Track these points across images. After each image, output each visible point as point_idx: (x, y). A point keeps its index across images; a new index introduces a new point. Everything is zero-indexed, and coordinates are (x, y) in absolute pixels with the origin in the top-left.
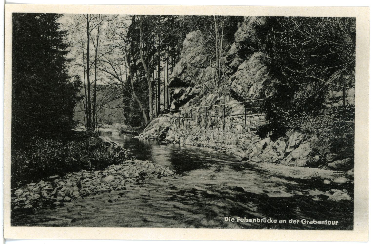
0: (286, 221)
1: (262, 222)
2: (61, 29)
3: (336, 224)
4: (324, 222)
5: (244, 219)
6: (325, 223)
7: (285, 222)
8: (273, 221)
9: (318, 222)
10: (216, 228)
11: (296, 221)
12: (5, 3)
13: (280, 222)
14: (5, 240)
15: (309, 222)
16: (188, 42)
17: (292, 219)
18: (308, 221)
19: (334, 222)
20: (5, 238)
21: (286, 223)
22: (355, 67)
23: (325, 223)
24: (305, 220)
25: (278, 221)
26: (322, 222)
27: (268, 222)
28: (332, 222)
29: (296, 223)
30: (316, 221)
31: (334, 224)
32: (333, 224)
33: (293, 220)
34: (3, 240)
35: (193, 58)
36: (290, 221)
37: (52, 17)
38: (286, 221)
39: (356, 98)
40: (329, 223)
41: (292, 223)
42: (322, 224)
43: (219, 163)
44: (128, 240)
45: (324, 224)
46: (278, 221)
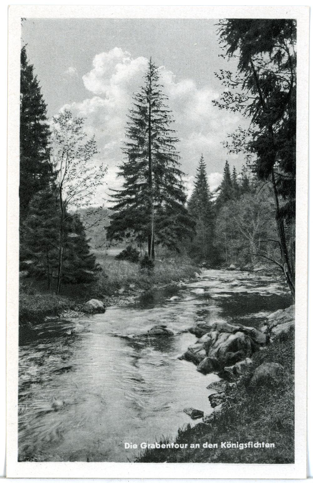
0: (216, 445)
2: (110, 220)
3: (186, 447)
5: (236, 444)
6: (262, 445)
7: (272, 445)
8: (226, 445)
11: (165, 446)
13: (191, 447)
14: (308, 477)
15: (150, 447)
16: (257, 63)
17: (207, 443)
19: (183, 445)
20: (305, 477)
21: (199, 447)
23: (262, 445)
25: (189, 446)
27: (255, 447)
28: (181, 445)
34: (309, 480)
35: (97, 224)
36: (204, 445)
38: (216, 445)
39: (300, 69)
40: (177, 446)
42: (233, 447)
43: (199, 350)
45: (235, 447)
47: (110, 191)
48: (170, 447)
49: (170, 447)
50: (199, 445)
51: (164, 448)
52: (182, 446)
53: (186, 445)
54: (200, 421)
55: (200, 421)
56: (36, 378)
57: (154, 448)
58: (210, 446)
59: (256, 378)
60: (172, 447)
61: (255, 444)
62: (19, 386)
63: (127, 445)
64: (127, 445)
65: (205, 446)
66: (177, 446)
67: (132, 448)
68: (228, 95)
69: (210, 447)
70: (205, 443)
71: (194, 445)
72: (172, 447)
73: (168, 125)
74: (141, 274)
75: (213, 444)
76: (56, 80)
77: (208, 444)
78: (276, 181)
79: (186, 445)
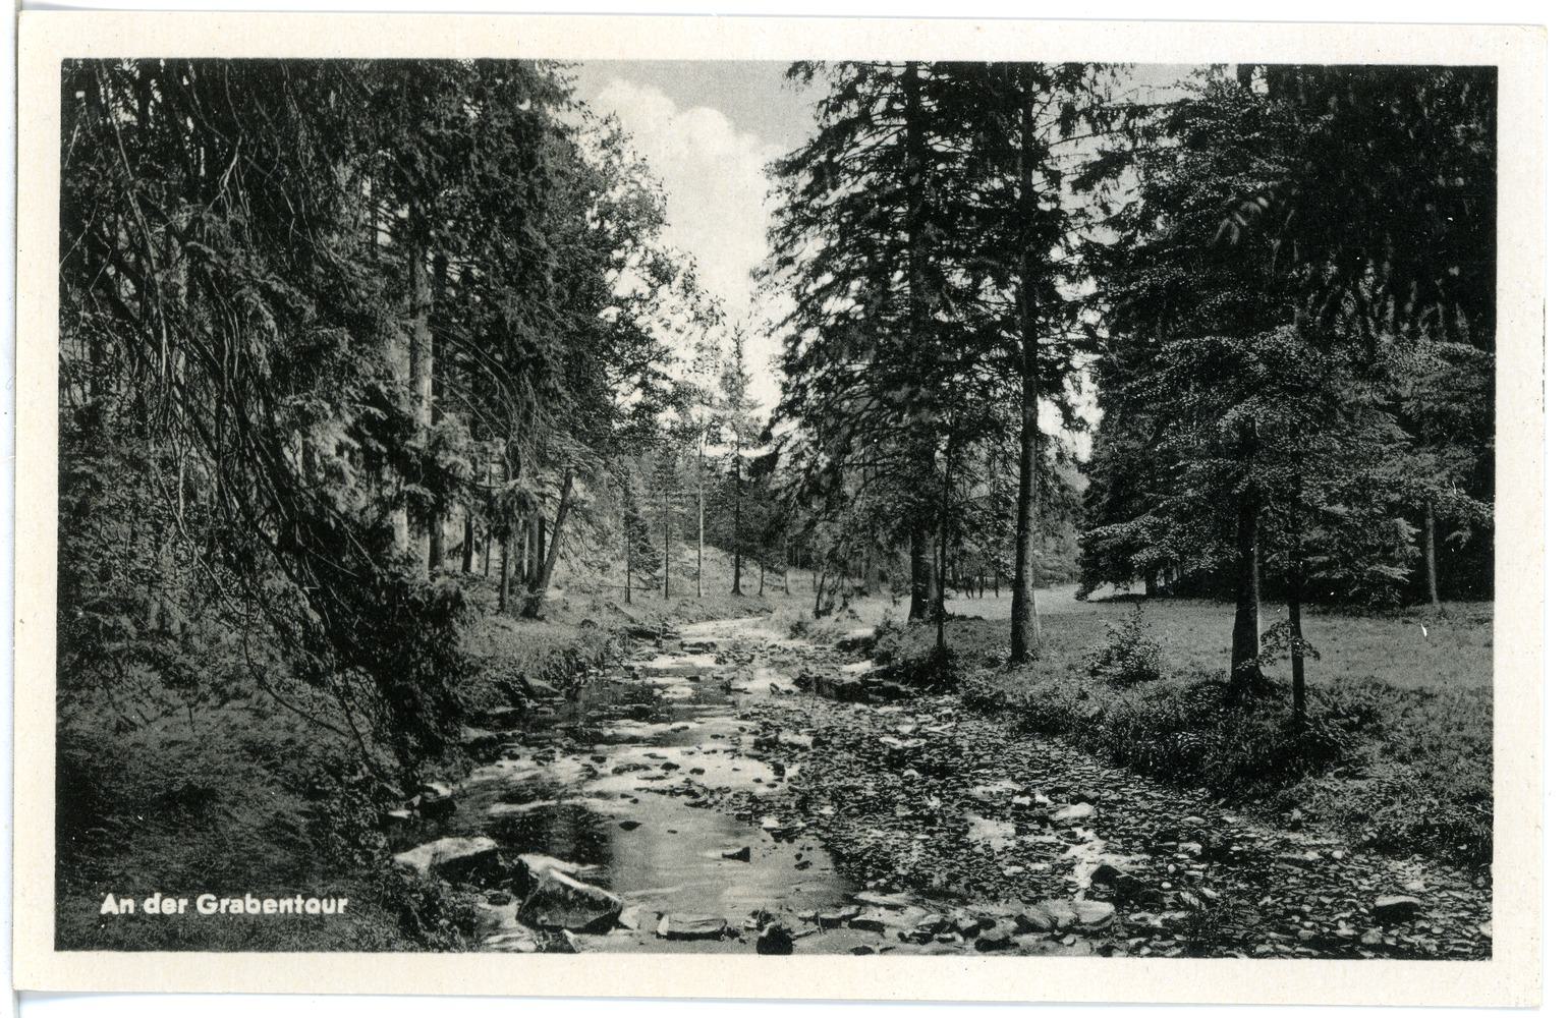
1: (223, 911)
4: (289, 902)
6: (295, 906)
9: (266, 902)
10: (711, 951)
12: (20, 8)
14: (19, 996)
15: (227, 908)
17: (157, 896)
18: (225, 902)
21: (131, 911)
22: (983, 64)
23: (295, 906)
24: (213, 898)
26: (283, 903)
29: (274, 911)
30: (256, 901)
31: (331, 911)
33: (305, 898)
34: (9, 997)
36: (149, 901)
37: (1042, 65)
41: (156, 910)
44: (684, 999)
46: (192, 906)
49: (290, 910)
50: (130, 903)
53: (183, 902)
54: (1135, 698)
55: (1135, 698)
56: (141, 707)
66: (313, 905)
67: (305, 912)
68: (141, 635)
69: (267, 911)
70: (152, 896)
73: (1190, 88)
74: (688, 425)
75: (277, 899)
79: (183, 902)
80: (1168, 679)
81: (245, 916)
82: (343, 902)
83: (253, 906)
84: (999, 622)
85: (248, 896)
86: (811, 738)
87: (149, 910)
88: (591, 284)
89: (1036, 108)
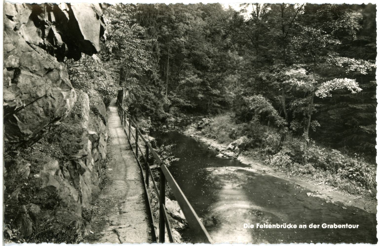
1: (328, 228)
4: (344, 225)
6: (346, 226)
11: (316, 226)
13: (300, 227)
15: (329, 227)
17: (312, 224)
18: (329, 225)
23: (346, 226)
24: (326, 224)
29: (271, 228)
32: (354, 227)
40: (350, 226)
41: (312, 227)
46: (298, 226)
47: (244, 3)
48: (345, 227)
49: (275, 227)
50: (306, 226)
51: (316, 228)
52: (354, 226)
57: (332, 227)
58: (315, 227)
59: (239, 194)
60: (347, 227)
61: (288, 225)
62: (292, 6)
63: (246, 226)
64: (246, 226)
65: (311, 226)
71: (302, 225)
72: (347, 227)
75: (272, 224)
76: (142, 45)
77: (313, 225)
78: (337, 54)
79: (319, 225)
80: (52, 165)
81: (334, 229)
82: (358, 226)
83: (278, 226)
84: (37, 30)
85: (277, 224)
86: (224, 34)
87: (310, 227)
88: (124, 202)
89: (46, 52)
